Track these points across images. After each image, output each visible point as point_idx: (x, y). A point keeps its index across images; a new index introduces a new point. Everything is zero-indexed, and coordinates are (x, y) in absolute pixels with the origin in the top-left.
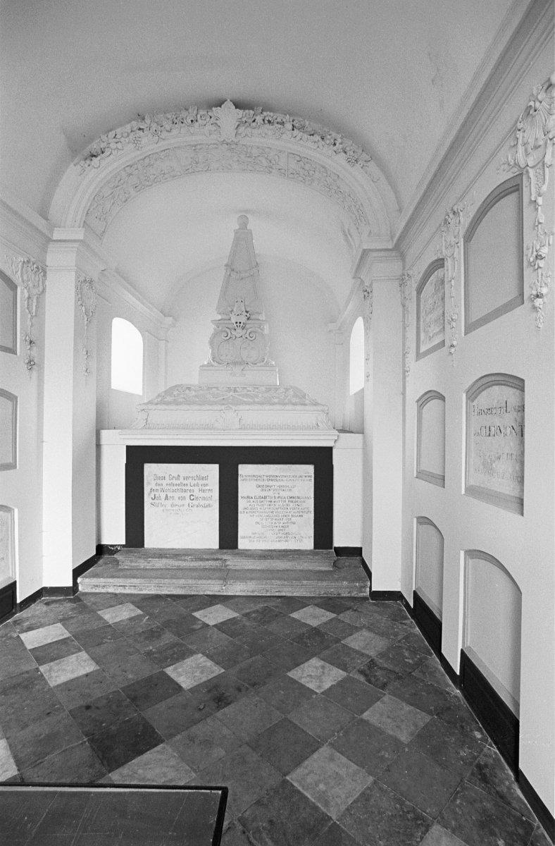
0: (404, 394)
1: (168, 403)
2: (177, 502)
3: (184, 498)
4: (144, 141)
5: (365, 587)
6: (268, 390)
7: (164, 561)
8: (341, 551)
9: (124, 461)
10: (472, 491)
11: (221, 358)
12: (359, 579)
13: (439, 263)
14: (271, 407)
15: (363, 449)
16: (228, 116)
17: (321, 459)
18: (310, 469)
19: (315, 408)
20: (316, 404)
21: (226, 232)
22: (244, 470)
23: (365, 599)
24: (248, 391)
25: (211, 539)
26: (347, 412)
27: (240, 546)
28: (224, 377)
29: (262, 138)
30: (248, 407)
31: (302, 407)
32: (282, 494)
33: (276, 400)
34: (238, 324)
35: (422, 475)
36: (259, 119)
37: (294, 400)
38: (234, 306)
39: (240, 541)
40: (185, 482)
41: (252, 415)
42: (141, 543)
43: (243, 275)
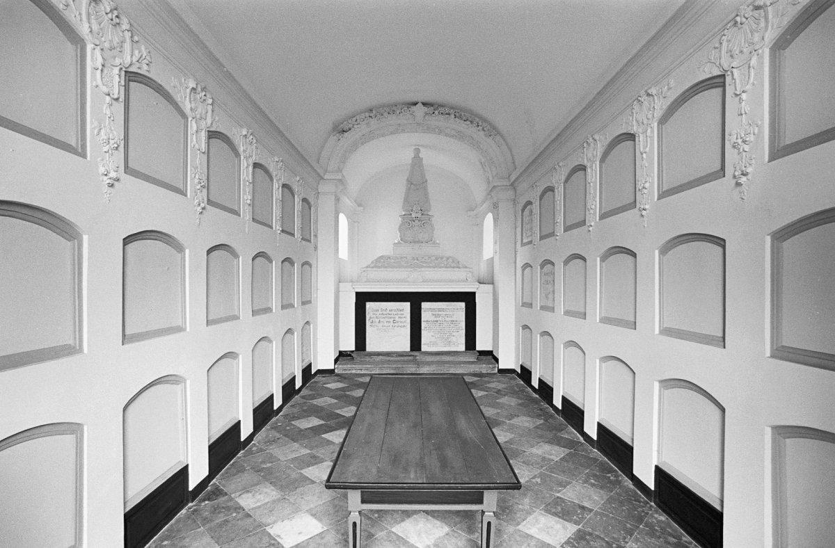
0: (515, 263)
1: (379, 267)
2: (386, 324)
3: (389, 322)
5: (495, 367)
6: (437, 259)
7: (381, 357)
8: (482, 353)
9: (354, 301)
10: (542, 308)
12: (492, 364)
13: (529, 203)
16: (419, 110)
17: (469, 299)
18: (463, 305)
19: (465, 269)
20: (466, 267)
21: (407, 156)
22: (425, 305)
23: (495, 374)
25: (406, 346)
26: (483, 270)
27: (423, 350)
28: (407, 250)
29: (437, 121)
31: (458, 269)
32: (447, 319)
35: (524, 305)
36: (436, 112)
37: (452, 265)
39: (422, 346)
40: (390, 313)
41: (429, 273)
42: (364, 349)
43: (418, 187)
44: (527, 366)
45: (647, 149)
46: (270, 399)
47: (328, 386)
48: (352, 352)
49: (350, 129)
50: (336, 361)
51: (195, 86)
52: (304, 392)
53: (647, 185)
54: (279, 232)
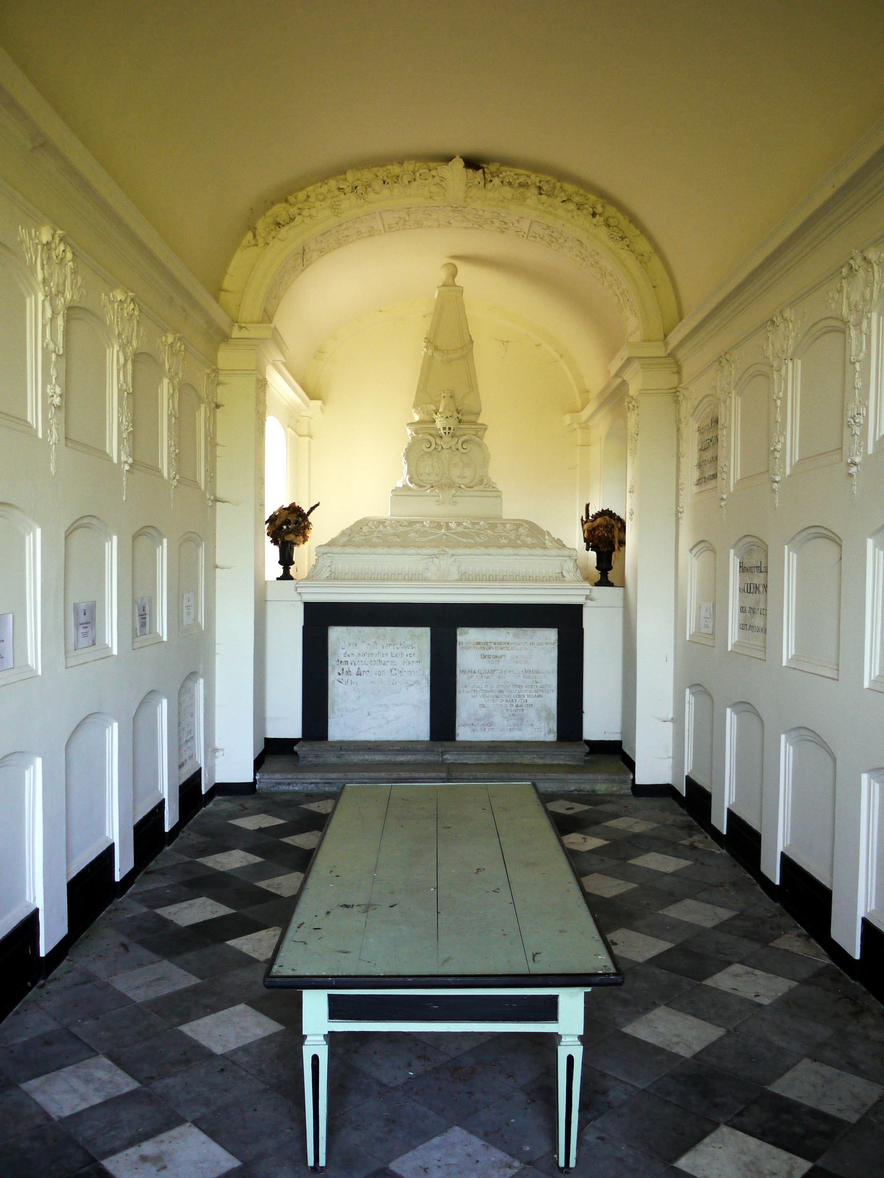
1: (359, 546)
4: (345, 204)
11: (422, 478)
14: (500, 551)
15: (624, 607)
24: (465, 528)
30: (466, 551)
33: (505, 541)
34: (447, 431)
38: (440, 402)
44: (702, 780)
45: (861, 356)
46: (107, 856)
47: (240, 822)
48: (294, 741)
49: (292, 219)
50: (258, 764)
51: (123, 299)
52: (188, 837)
53: (779, 447)
54: (127, 467)
